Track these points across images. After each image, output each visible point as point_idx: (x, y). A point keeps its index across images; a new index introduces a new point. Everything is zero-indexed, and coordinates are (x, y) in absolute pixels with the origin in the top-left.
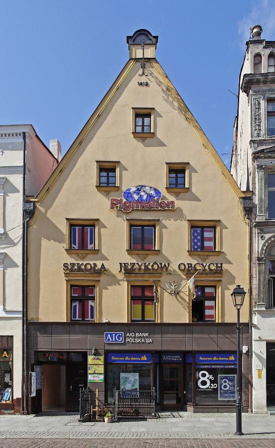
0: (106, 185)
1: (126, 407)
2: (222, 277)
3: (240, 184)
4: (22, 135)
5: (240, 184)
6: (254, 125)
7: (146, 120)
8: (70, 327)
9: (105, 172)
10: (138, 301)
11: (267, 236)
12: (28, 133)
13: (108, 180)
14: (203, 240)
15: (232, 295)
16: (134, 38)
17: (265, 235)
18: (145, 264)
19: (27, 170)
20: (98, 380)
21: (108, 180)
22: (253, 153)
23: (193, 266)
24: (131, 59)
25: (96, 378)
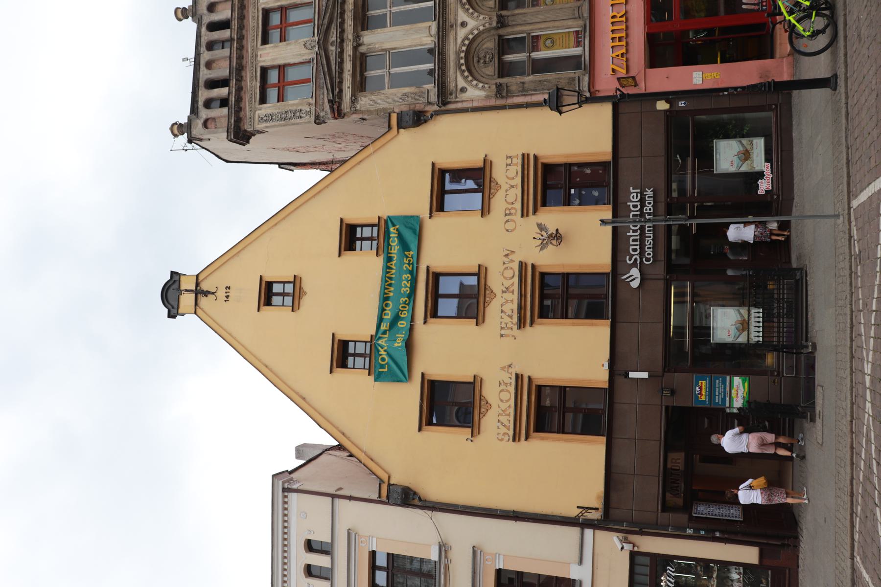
0: (367, 359)
1: (779, 332)
2: (528, 155)
3: (508, 250)
4: (286, 494)
5: (508, 250)
6: (293, 121)
7: (277, 288)
8: (618, 322)
9: (347, 359)
10: (276, 12)
11: (461, 83)
12: (283, 483)
13: (360, 355)
14: (663, 393)
15: (561, 113)
16: (170, 307)
17: (459, 87)
18: (503, 292)
19: (339, 493)
20: (744, 389)
21: (360, 355)
22: (335, 118)
23: (510, 206)
24: (195, 313)
25: (740, 394)
